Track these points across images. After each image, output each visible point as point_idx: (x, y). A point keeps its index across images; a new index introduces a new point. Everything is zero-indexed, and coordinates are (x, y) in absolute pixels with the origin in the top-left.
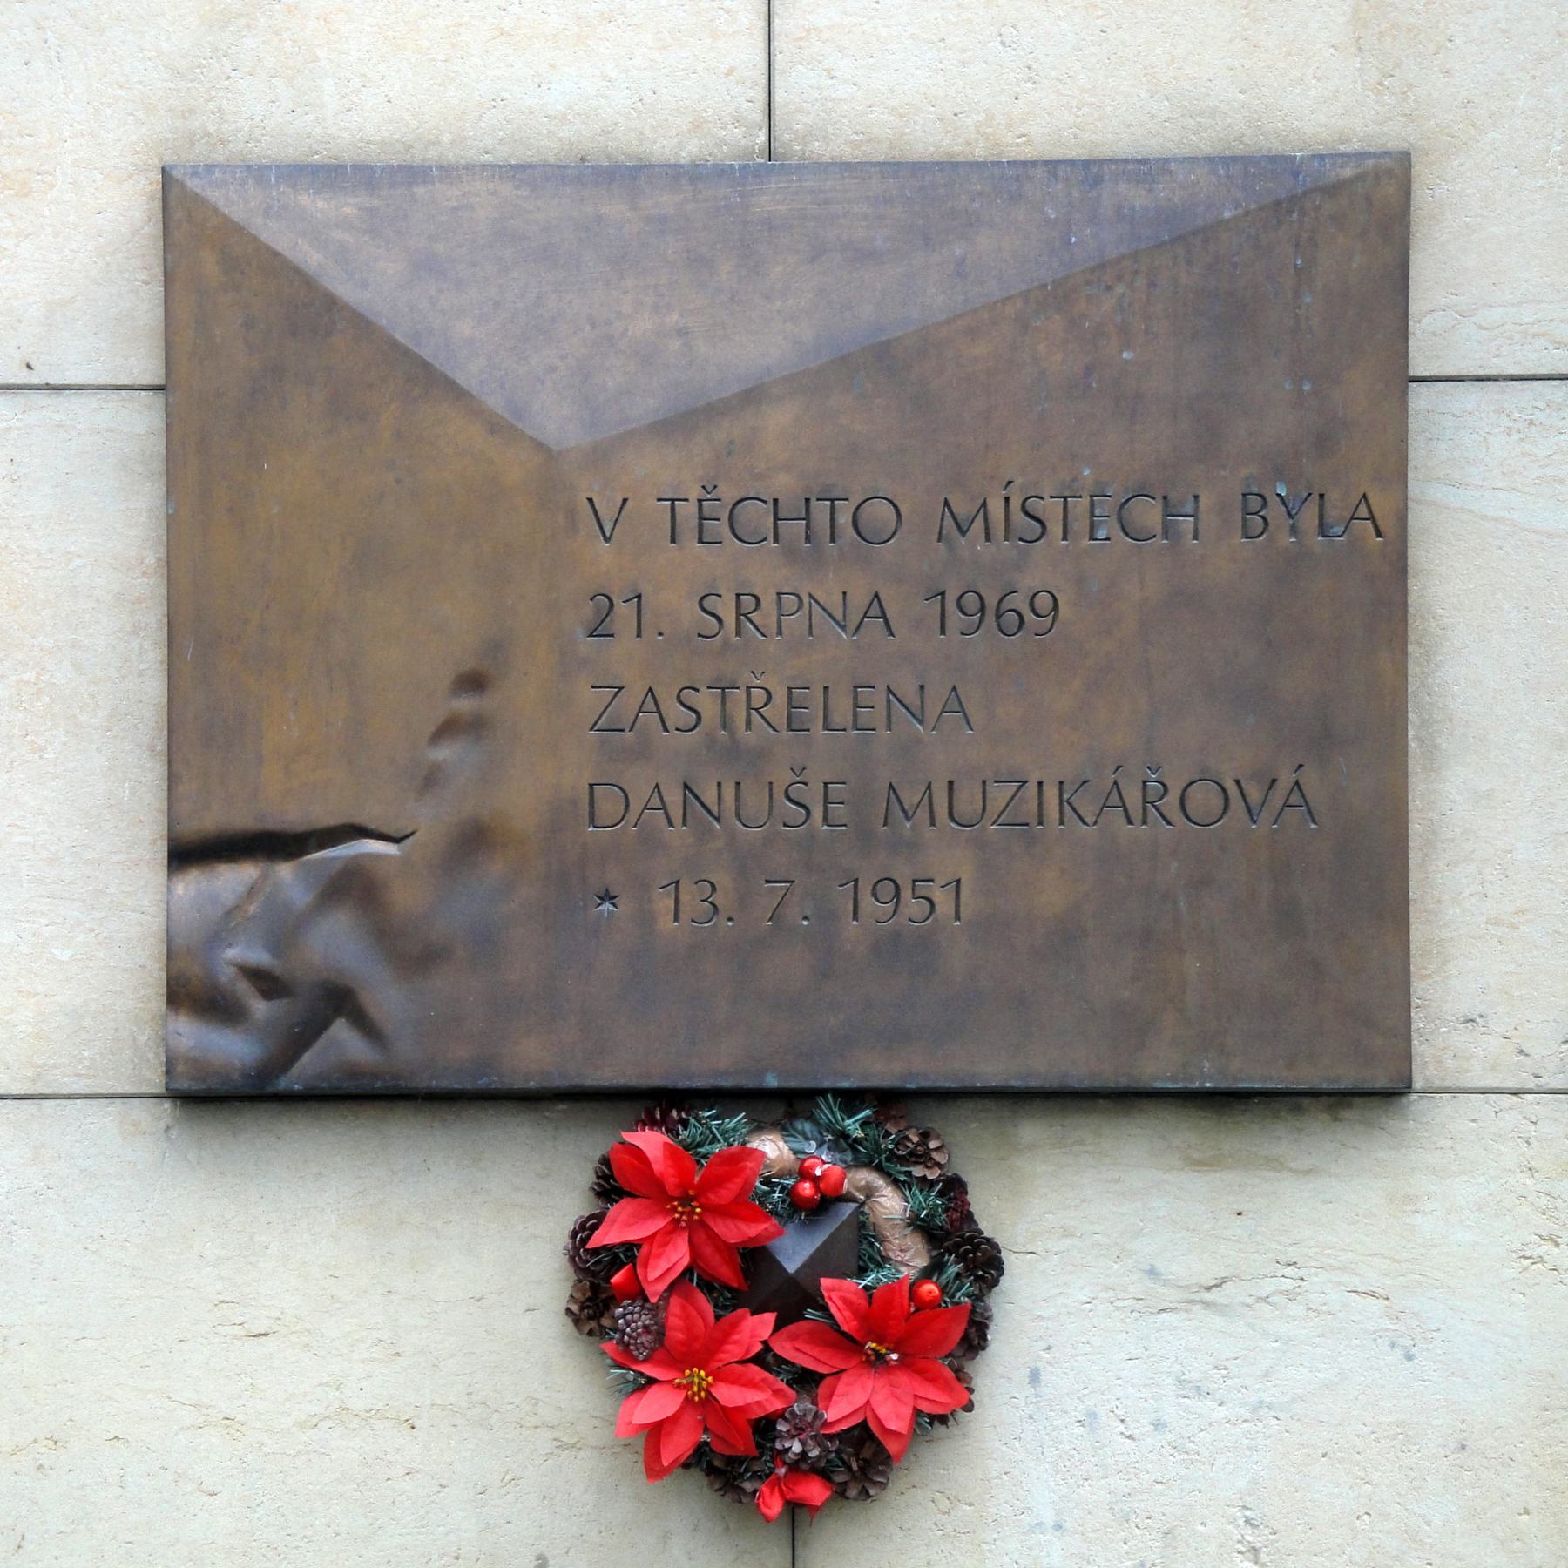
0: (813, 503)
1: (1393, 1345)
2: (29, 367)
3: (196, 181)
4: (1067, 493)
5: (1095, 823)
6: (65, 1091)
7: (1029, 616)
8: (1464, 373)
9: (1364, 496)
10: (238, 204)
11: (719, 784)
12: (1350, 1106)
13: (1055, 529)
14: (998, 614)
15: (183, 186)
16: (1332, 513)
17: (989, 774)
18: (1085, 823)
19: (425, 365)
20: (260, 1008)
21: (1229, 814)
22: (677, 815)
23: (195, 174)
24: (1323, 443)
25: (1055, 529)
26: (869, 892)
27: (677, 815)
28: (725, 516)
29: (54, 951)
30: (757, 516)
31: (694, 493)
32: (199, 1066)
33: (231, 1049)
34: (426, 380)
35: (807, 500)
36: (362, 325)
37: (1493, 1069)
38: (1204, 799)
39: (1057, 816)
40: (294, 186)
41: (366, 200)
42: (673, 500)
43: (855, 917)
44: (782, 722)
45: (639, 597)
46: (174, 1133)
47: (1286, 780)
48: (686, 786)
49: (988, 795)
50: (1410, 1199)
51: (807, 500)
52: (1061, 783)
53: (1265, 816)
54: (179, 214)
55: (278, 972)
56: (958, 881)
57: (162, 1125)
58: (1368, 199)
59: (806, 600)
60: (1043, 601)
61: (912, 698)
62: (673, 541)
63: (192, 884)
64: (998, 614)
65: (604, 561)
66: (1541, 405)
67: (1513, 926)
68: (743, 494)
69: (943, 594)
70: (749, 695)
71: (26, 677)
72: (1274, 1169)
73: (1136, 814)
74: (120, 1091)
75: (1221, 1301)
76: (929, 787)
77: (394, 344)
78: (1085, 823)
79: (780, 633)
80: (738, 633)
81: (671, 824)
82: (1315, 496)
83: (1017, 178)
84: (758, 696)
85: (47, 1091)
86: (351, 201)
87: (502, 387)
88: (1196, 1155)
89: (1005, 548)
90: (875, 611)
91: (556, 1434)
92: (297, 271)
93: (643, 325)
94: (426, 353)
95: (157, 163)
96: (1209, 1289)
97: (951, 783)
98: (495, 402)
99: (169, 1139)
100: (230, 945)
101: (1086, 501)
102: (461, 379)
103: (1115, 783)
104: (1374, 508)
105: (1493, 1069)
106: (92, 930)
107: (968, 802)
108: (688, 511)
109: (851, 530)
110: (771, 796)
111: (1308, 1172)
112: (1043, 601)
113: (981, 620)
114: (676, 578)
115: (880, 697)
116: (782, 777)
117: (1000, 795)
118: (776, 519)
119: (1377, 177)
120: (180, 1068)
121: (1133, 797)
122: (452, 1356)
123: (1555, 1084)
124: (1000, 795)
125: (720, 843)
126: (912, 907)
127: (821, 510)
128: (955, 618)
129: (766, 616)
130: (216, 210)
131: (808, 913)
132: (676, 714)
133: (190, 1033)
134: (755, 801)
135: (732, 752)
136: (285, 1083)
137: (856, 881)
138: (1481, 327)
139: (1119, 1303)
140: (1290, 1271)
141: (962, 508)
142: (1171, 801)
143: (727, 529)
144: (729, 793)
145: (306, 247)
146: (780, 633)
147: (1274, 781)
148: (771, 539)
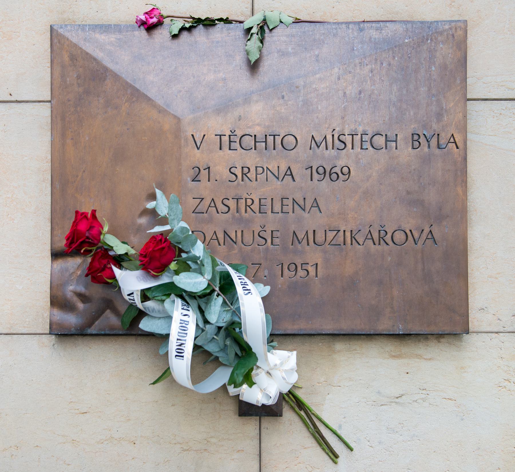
0: (268, 136)
1: (457, 415)
2: (11, 95)
3: (62, 30)
4: (353, 133)
5: (363, 244)
6: (20, 332)
7: (340, 174)
8: (479, 98)
9: (453, 135)
10: (74, 37)
11: (236, 231)
12: (443, 337)
13: (349, 146)
14: (329, 174)
15: (57, 31)
16: (442, 142)
17: (327, 228)
18: (359, 244)
19: (138, 90)
20: (81, 306)
21: (408, 241)
22: (222, 241)
23: (61, 27)
24: (439, 116)
25: (349, 146)
26: (287, 268)
27: (222, 241)
28: (238, 141)
29: (17, 286)
30: (248, 141)
31: (228, 133)
32: (60, 325)
33: (71, 320)
34: (136, 95)
35: (266, 135)
36: (116, 77)
37: (490, 325)
38: (399, 237)
39: (350, 242)
40: (94, 32)
41: (119, 36)
42: (220, 135)
43: (282, 276)
44: (257, 210)
45: (209, 168)
46: (56, 346)
47: (427, 230)
48: (225, 232)
49: (327, 235)
50: (462, 368)
51: (266, 135)
52: (351, 231)
53: (420, 243)
54: (56, 41)
55: (87, 294)
56: (317, 264)
57: (52, 344)
58: (453, 36)
59: (265, 169)
60: (345, 170)
61: (302, 203)
62: (221, 149)
63: (60, 264)
64: (329, 174)
65: (198, 157)
66: (504, 108)
67: (496, 278)
68: (244, 134)
69: (311, 167)
70: (246, 201)
71: (8, 196)
72: (419, 358)
73: (377, 242)
74: (38, 332)
75: (402, 402)
76: (307, 232)
77: (127, 83)
78: (359, 244)
79: (256, 180)
80: (242, 180)
81: (220, 245)
82: (436, 135)
83: (336, 29)
84: (249, 202)
85: (14, 332)
86: (113, 36)
87: (163, 97)
88: (393, 354)
89: (334, 152)
90: (289, 173)
91: (182, 446)
92: (95, 59)
93: (211, 77)
94: (137, 86)
95: (50, 25)
96: (397, 398)
97: (314, 231)
98: (160, 102)
99: (54, 348)
100: (71, 285)
101: (359, 136)
102: (149, 95)
103: (370, 231)
104: (456, 139)
105: (490, 325)
106: (29, 279)
107: (320, 237)
108: (225, 139)
109: (280, 146)
110: (253, 235)
111: (430, 359)
112: (345, 170)
113: (324, 176)
114: (222, 161)
115: (290, 202)
116: (258, 229)
117: (331, 235)
118: (255, 142)
119: (456, 29)
120: (54, 327)
121: (376, 236)
122: (147, 420)
123: (509, 330)
124: (331, 235)
125: (236, 251)
126: (301, 273)
127: (270, 139)
128: (315, 176)
129: (252, 175)
130: (68, 39)
131: (266, 274)
132: (222, 208)
133: (59, 315)
134: (248, 238)
135: (240, 220)
136: (89, 331)
137: (282, 264)
138: (484, 83)
139: (368, 403)
140: (424, 392)
141: (318, 139)
142: (388, 238)
143: (239, 145)
144: (239, 234)
145: (98, 51)
146: (256, 180)
147: (423, 230)
148: (253, 148)
